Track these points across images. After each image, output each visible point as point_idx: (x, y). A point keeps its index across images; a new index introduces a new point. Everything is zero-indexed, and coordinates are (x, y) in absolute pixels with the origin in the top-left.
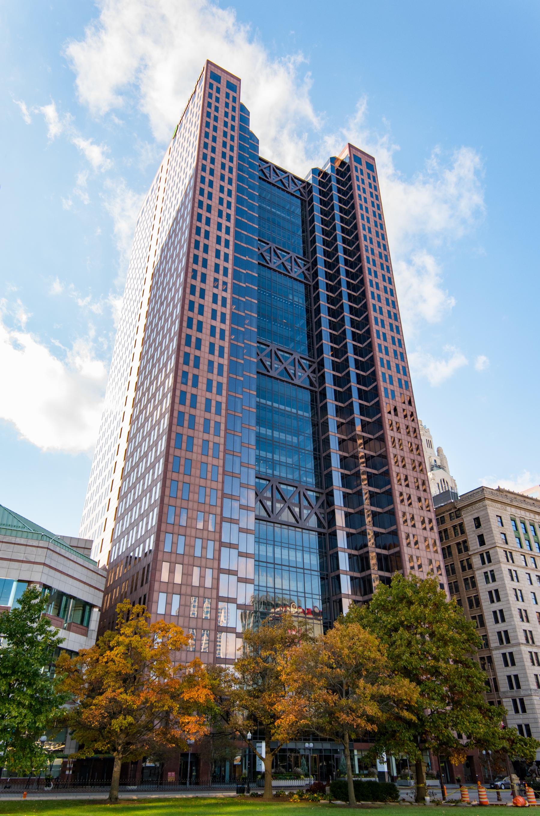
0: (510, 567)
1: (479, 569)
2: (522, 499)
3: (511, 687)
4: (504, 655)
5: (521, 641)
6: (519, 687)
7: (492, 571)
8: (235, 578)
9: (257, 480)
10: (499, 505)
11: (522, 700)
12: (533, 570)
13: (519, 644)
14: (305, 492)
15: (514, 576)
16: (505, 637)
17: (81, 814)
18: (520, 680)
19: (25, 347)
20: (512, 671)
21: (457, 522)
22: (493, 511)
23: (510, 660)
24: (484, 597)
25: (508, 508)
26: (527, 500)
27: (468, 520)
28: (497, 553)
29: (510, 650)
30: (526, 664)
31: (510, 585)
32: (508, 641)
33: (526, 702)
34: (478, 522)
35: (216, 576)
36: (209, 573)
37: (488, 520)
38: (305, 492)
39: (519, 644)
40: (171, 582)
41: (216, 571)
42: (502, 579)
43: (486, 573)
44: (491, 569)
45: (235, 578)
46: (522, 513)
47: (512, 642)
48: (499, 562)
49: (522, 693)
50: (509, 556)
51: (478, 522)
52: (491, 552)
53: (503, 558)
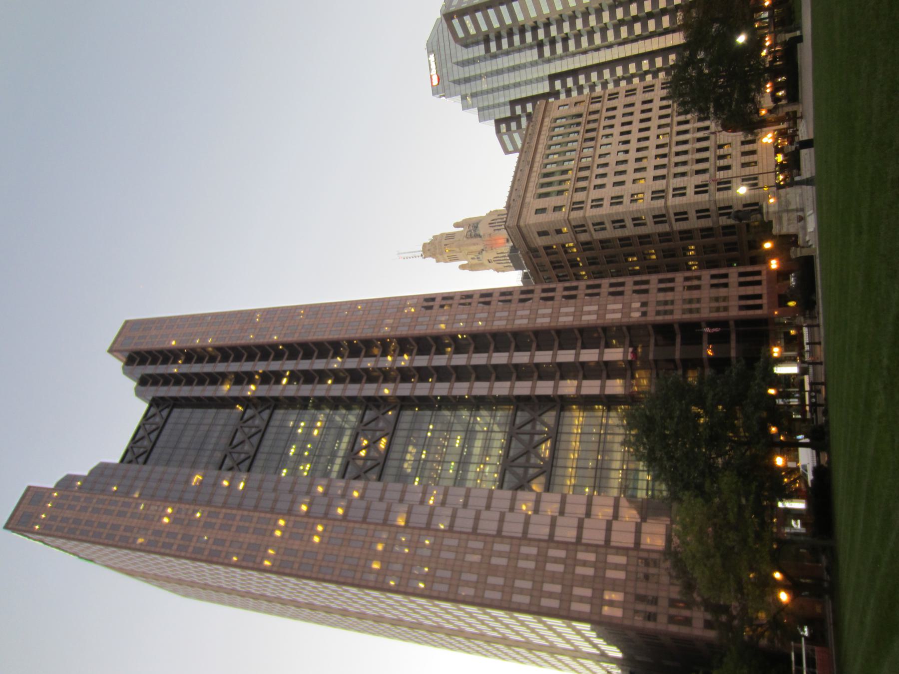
0: (589, 206)
1: (591, 235)
2: (519, 172)
3: (708, 216)
4: (677, 220)
5: (663, 204)
6: (707, 210)
7: (594, 225)
8: (586, 520)
9: (505, 485)
10: (525, 210)
11: (720, 209)
12: (595, 151)
13: (666, 207)
14: (516, 426)
15: (597, 203)
16: (659, 218)
17: (820, 302)
18: (700, 208)
19: (435, 91)
20: (692, 215)
21: (542, 252)
22: (531, 219)
23: (682, 216)
24: (620, 233)
25: (527, 200)
26: (517, 178)
27: (541, 242)
28: (575, 219)
29: (672, 216)
30: (685, 202)
31: (607, 209)
32: (663, 216)
33: (722, 205)
34: (542, 234)
35: (583, 548)
36: (581, 556)
37: (541, 224)
38: (516, 426)
39: (666, 207)
40: (621, 311)
41: (579, 547)
42: (601, 216)
43: (595, 230)
44: (591, 226)
45: (586, 520)
46: (532, 185)
47: (664, 212)
48: (584, 217)
49: (713, 208)
50: (577, 206)
51: (542, 234)
52: (573, 224)
53: (580, 213)
